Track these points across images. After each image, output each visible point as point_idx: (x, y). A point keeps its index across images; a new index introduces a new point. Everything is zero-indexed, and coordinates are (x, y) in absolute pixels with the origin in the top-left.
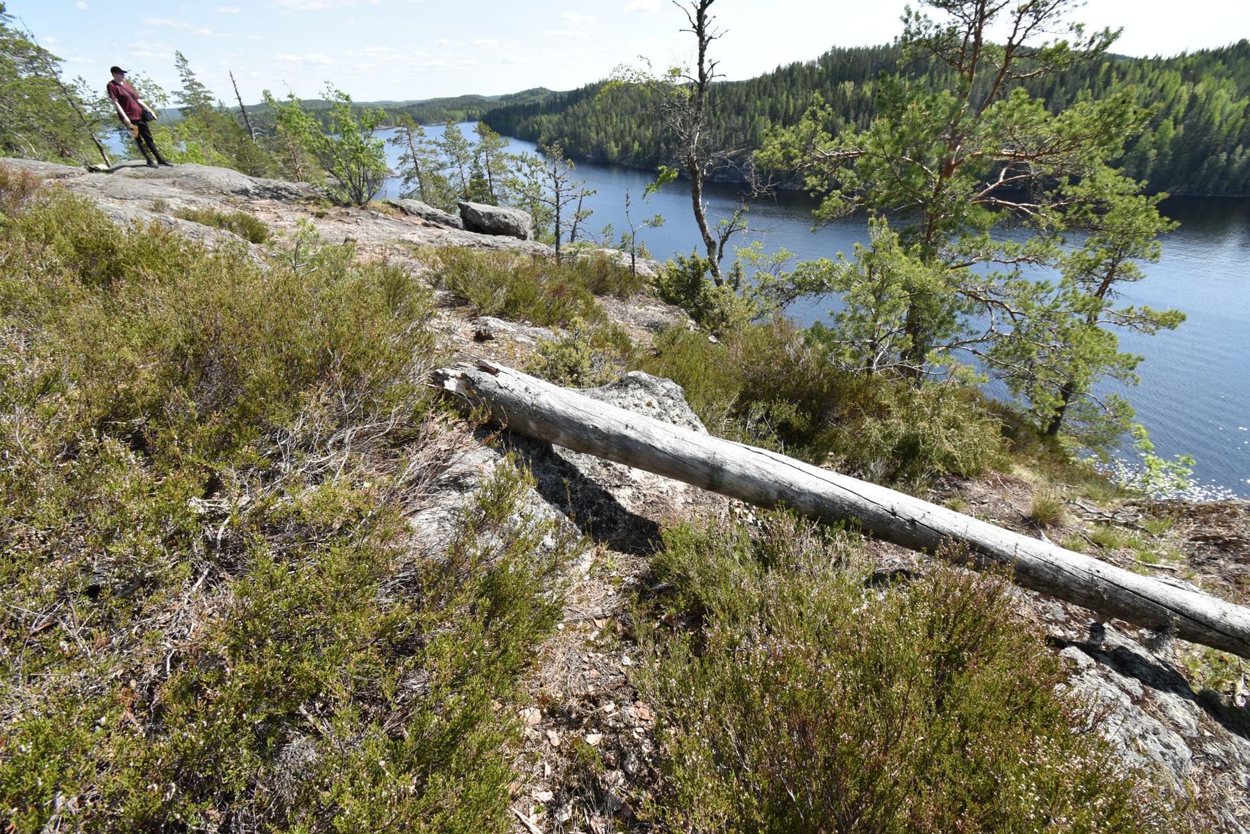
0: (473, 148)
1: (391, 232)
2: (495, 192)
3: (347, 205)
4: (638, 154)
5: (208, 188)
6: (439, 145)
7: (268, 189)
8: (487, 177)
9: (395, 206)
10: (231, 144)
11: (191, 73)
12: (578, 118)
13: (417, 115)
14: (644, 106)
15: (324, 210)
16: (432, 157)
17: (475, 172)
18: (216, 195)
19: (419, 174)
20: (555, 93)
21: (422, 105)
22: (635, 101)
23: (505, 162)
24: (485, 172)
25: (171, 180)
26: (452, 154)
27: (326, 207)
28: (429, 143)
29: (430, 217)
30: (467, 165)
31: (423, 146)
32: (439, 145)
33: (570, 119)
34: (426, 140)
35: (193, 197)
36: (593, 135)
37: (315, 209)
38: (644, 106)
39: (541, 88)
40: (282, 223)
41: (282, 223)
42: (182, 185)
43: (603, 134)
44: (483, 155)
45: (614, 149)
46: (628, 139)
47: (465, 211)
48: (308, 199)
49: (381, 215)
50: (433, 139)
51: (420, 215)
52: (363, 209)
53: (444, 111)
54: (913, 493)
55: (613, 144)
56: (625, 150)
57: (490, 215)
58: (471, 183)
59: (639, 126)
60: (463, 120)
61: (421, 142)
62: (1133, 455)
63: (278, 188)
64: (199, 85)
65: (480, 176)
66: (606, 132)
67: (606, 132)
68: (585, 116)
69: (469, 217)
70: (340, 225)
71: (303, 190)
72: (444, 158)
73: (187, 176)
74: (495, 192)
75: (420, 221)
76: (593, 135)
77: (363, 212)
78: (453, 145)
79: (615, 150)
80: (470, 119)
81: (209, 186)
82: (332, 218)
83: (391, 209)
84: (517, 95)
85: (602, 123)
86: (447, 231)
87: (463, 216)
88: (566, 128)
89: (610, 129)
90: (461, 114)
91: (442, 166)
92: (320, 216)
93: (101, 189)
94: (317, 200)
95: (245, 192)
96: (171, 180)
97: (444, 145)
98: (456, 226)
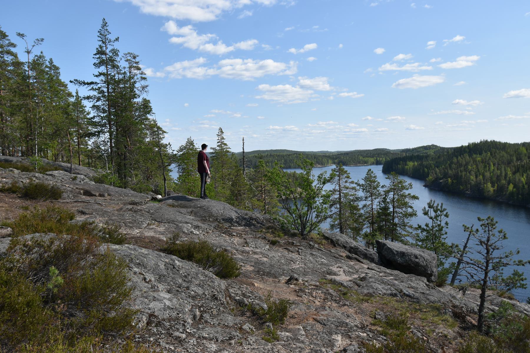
0: (384, 189)
1: (322, 264)
2: (396, 220)
3: (294, 235)
4: (512, 194)
5: (210, 217)
6: (359, 185)
7: (245, 219)
8: (391, 210)
9: (326, 238)
10: (231, 177)
11: (223, 138)
12: (461, 165)
13: (343, 160)
14: (519, 159)
15: (277, 239)
16: (352, 192)
17: (383, 205)
18: (212, 222)
19: (340, 203)
20: (443, 149)
21: (347, 154)
22: (511, 156)
23: (407, 200)
24: (391, 206)
25: (189, 210)
26: (367, 192)
27: (279, 236)
28: (352, 182)
29: (353, 250)
30: (377, 200)
31: (347, 185)
32: (359, 185)
33: (454, 166)
34: (350, 180)
35: (200, 224)
36: (472, 177)
37: (270, 236)
38: (519, 159)
39: (433, 145)
40: (247, 249)
41: (247, 249)
42: (196, 214)
43: (481, 177)
44: (391, 195)
45: (490, 188)
46: (504, 182)
47: (381, 247)
48: (268, 228)
49: (316, 246)
50: (356, 181)
51: (345, 247)
52: (304, 239)
53: (361, 158)
54: (231, 59)
55: (489, 185)
56: (501, 190)
57: (403, 254)
58: (378, 213)
59: (514, 173)
60: (373, 164)
61: (346, 182)
62: (191, 29)
63: (251, 219)
64: (225, 144)
65: (386, 209)
66: (484, 176)
67: (484, 176)
68: (467, 164)
69: (385, 253)
70: (286, 253)
71: (267, 220)
72: (361, 194)
73: (200, 207)
74: (396, 220)
75: (344, 253)
76: (472, 177)
77: (304, 243)
78: (370, 185)
79: (491, 189)
80: (378, 163)
81: (211, 215)
82: (281, 246)
83: (324, 241)
84: (414, 149)
85: (481, 170)
86: (365, 265)
87: (379, 252)
88: (450, 172)
89: (487, 174)
90: (372, 160)
91: (358, 199)
92: (273, 243)
93: (152, 214)
94: (272, 229)
95: (230, 220)
96: (189, 210)
97: (363, 185)
98: (372, 260)
